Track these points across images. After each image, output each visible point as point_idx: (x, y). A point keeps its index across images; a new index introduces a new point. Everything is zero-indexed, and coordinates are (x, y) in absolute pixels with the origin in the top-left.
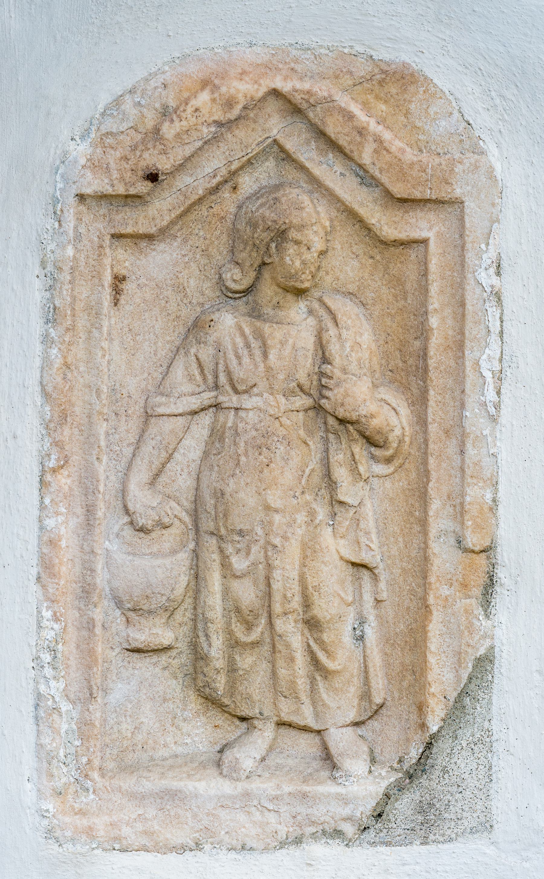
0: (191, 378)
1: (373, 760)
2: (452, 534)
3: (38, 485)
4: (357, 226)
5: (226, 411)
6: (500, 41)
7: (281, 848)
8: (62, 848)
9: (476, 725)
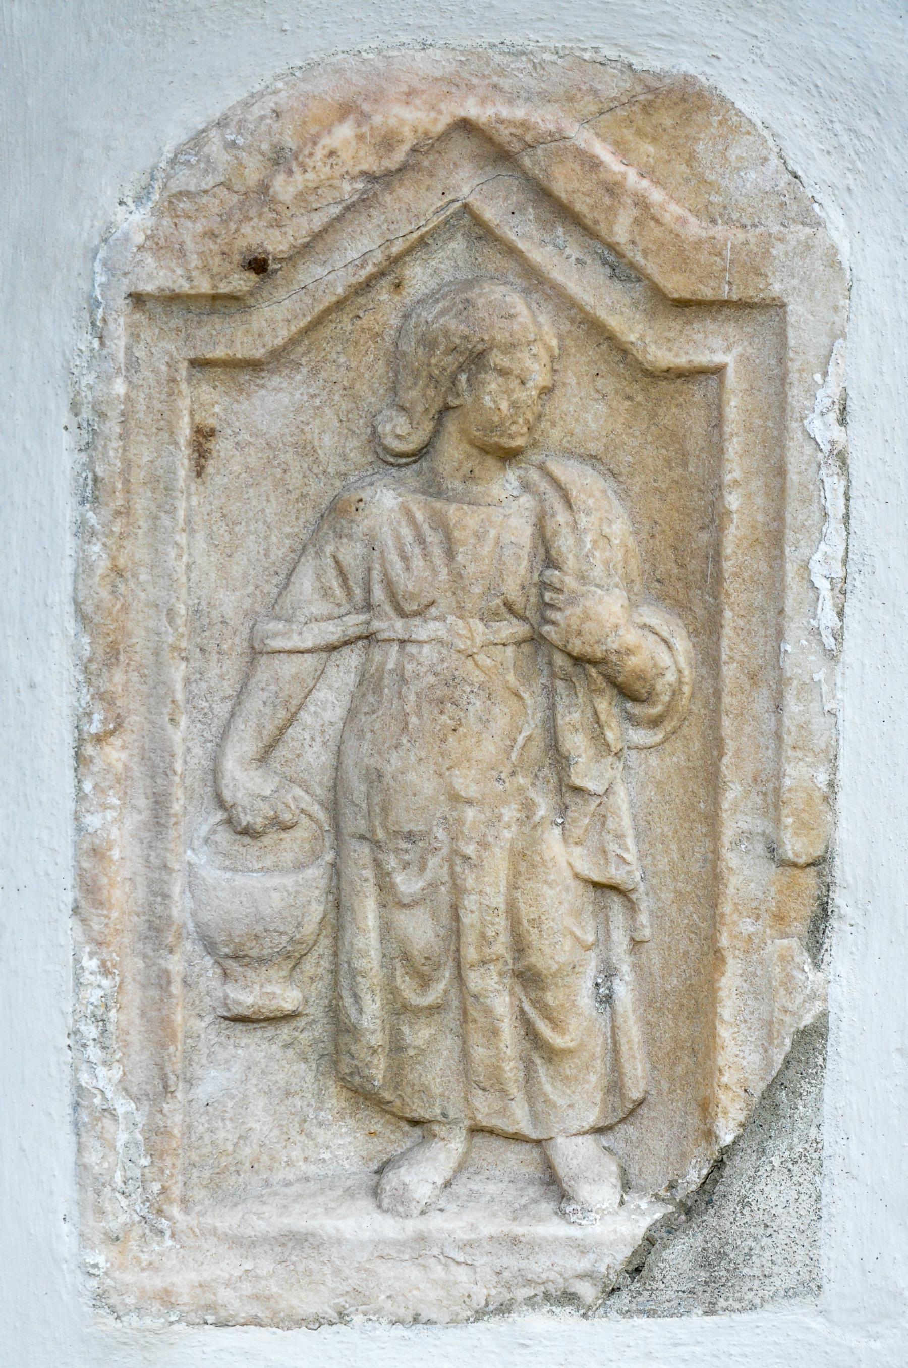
0: (326, 593)
1: (626, 1186)
2: (761, 838)
3: (73, 762)
5: (385, 646)
6: (850, 39)
7: (477, 1320)
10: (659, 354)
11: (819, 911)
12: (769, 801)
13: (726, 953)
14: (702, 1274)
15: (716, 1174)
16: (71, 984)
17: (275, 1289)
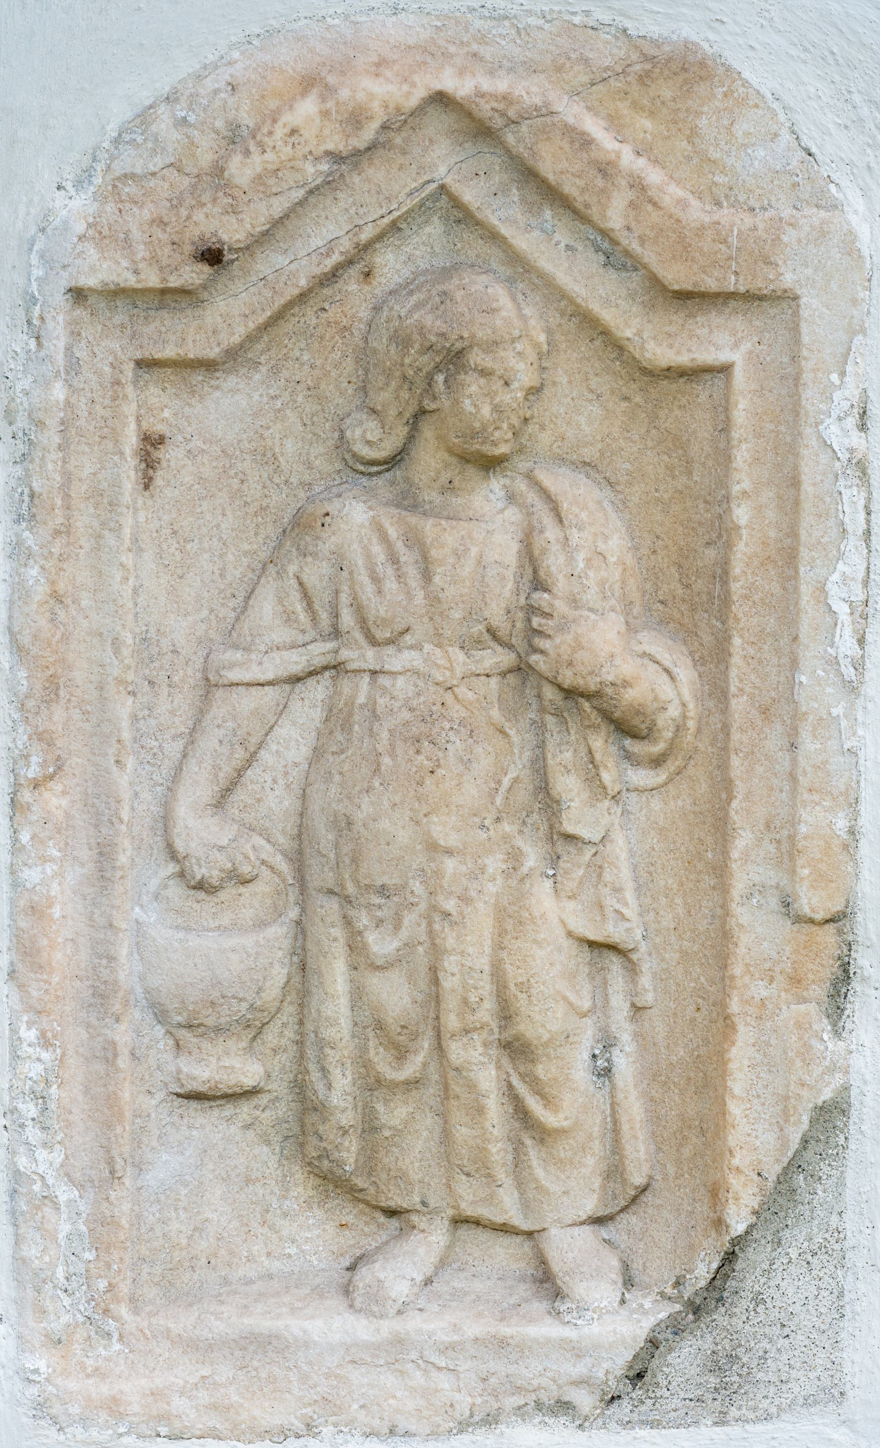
1: (629, 1282)
3: (8, 810)
7: (461, 1432)
11: (840, 972)
13: (736, 1020)
14: (712, 1379)
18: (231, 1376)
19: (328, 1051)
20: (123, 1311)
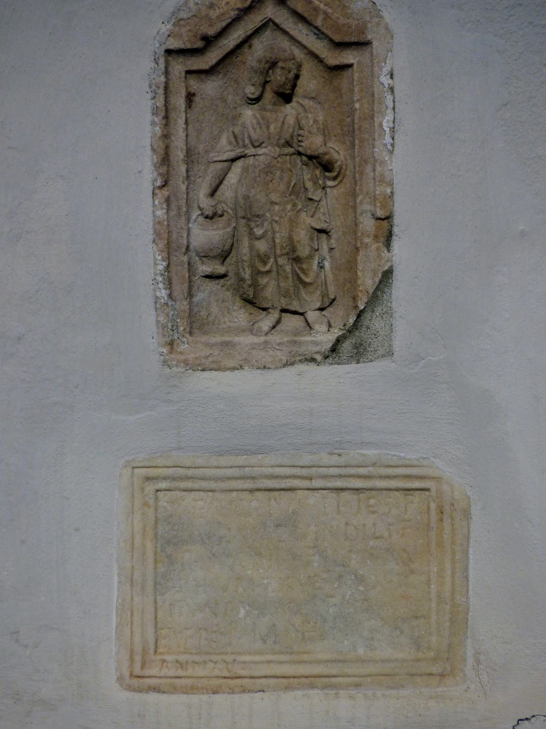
0: (230, 143)
1: (330, 326)
2: (370, 212)
3: (151, 195)
4: (315, 61)
5: (249, 158)
7: (284, 367)
8: (172, 370)
9: (384, 305)
10: (332, 61)
11: (389, 234)
12: (372, 200)
13: (359, 249)
14: (355, 351)
15: (358, 319)
16: (153, 264)
17: (220, 359)
18: (218, 353)
19: (245, 263)
20: (187, 335)
